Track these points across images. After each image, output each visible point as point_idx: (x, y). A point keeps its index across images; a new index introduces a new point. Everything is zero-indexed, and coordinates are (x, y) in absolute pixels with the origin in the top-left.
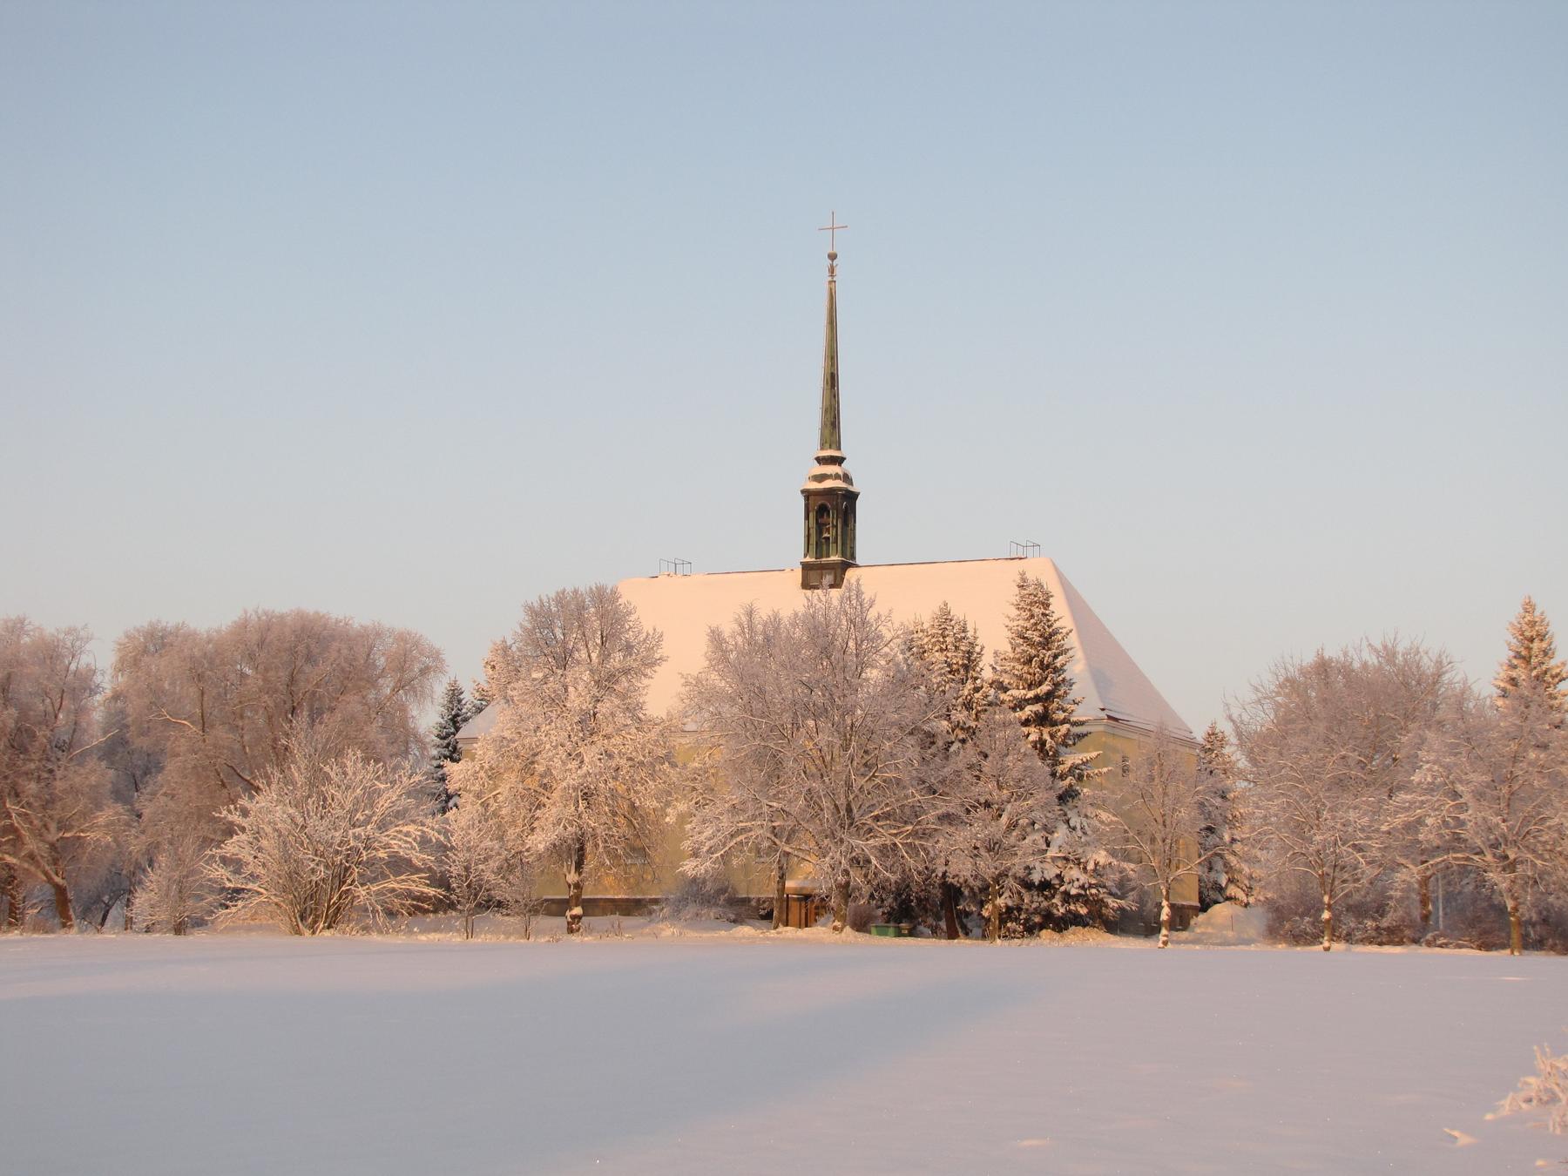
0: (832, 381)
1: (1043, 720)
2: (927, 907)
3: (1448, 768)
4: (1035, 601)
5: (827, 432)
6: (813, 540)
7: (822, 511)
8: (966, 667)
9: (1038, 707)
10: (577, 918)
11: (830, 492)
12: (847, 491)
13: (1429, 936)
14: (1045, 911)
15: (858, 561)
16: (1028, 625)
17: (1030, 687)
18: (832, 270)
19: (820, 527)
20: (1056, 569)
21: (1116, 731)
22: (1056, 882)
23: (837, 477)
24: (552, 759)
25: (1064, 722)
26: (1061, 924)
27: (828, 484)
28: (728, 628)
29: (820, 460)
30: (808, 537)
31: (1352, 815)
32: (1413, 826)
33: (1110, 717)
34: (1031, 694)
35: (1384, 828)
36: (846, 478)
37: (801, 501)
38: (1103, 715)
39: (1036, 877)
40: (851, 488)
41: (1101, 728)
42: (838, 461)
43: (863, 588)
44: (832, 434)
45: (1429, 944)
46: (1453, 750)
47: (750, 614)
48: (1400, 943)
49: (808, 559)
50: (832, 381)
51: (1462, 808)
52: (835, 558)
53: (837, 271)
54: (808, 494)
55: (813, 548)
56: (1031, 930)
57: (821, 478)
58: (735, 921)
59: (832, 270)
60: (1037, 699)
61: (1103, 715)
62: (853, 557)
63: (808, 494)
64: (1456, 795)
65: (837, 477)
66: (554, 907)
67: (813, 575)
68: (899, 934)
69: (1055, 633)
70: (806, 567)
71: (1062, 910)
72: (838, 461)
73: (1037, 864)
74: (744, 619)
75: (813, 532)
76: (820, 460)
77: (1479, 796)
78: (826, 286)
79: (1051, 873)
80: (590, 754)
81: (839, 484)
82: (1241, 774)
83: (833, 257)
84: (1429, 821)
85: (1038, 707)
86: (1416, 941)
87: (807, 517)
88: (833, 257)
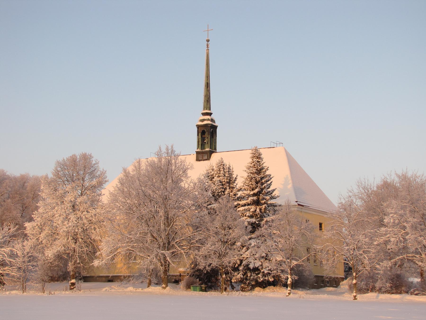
0: (208, 85)
1: (257, 203)
2: (207, 279)
3: (401, 216)
5: (205, 104)
6: (200, 143)
7: (203, 133)
8: (229, 183)
9: (255, 198)
10: (73, 284)
11: (206, 125)
12: (212, 125)
13: (412, 290)
14: (255, 280)
15: (218, 151)
16: (252, 166)
18: (208, 46)
19: (203, 139)
20: (285, 149)
21: (303, 210)
22: (260, 268)
23: (208, 120)
24: (58, 221)
25: (265, 203)
26: (264, 285)
27: (205, 122)
28: (130, 169)
29: (204, 114)
30: (198, 142)
31: (361, 237)
32: (386, 242)
33: (299, 205)
34: (252, 193)
35: (375, 243)
36: (212, 120)
37: (196, 129)
38: (296, 204)
39: (251, 266)
40: (214, 124)
41: (296, 209)
42: (210, 114)
43: (174, 149)
44: (207, 105)
45: (412, 294)
46: (403, 208)
47: (139, 162)
48: (400, 293)
49: (198, 150)
50: (208, 85)
51: (407, 234)
52: (207, 149)
53: (209, 46)
54: (198, 126)
55: (200, 146)
56: (253, 288)
57: (202, 120)
58: (157, 284)
59: (208, 46)
60: (254, 195)
61: (296, 204)
62: (215, 149)
63: (198, 126)
64: (404, 228)
65: (208, 120)
66: (104, 279)
67: (200, 156)
68: (202, 290)
69: (263, 169)
70: (198, 153)
71: (262, 279)
72: (210, 114)
73: (252, 261)
74: (137, 164)
75: (200, 140)
76: (204, 114)
77: (414, 228)
79: (258, 264)
80: (72, 217)
81: (209, 122)
83: (208, 41)
84: (392, 239)
85: (255, 198)
86: (407, 292)
87: (198, 135)
88: (208, 41)
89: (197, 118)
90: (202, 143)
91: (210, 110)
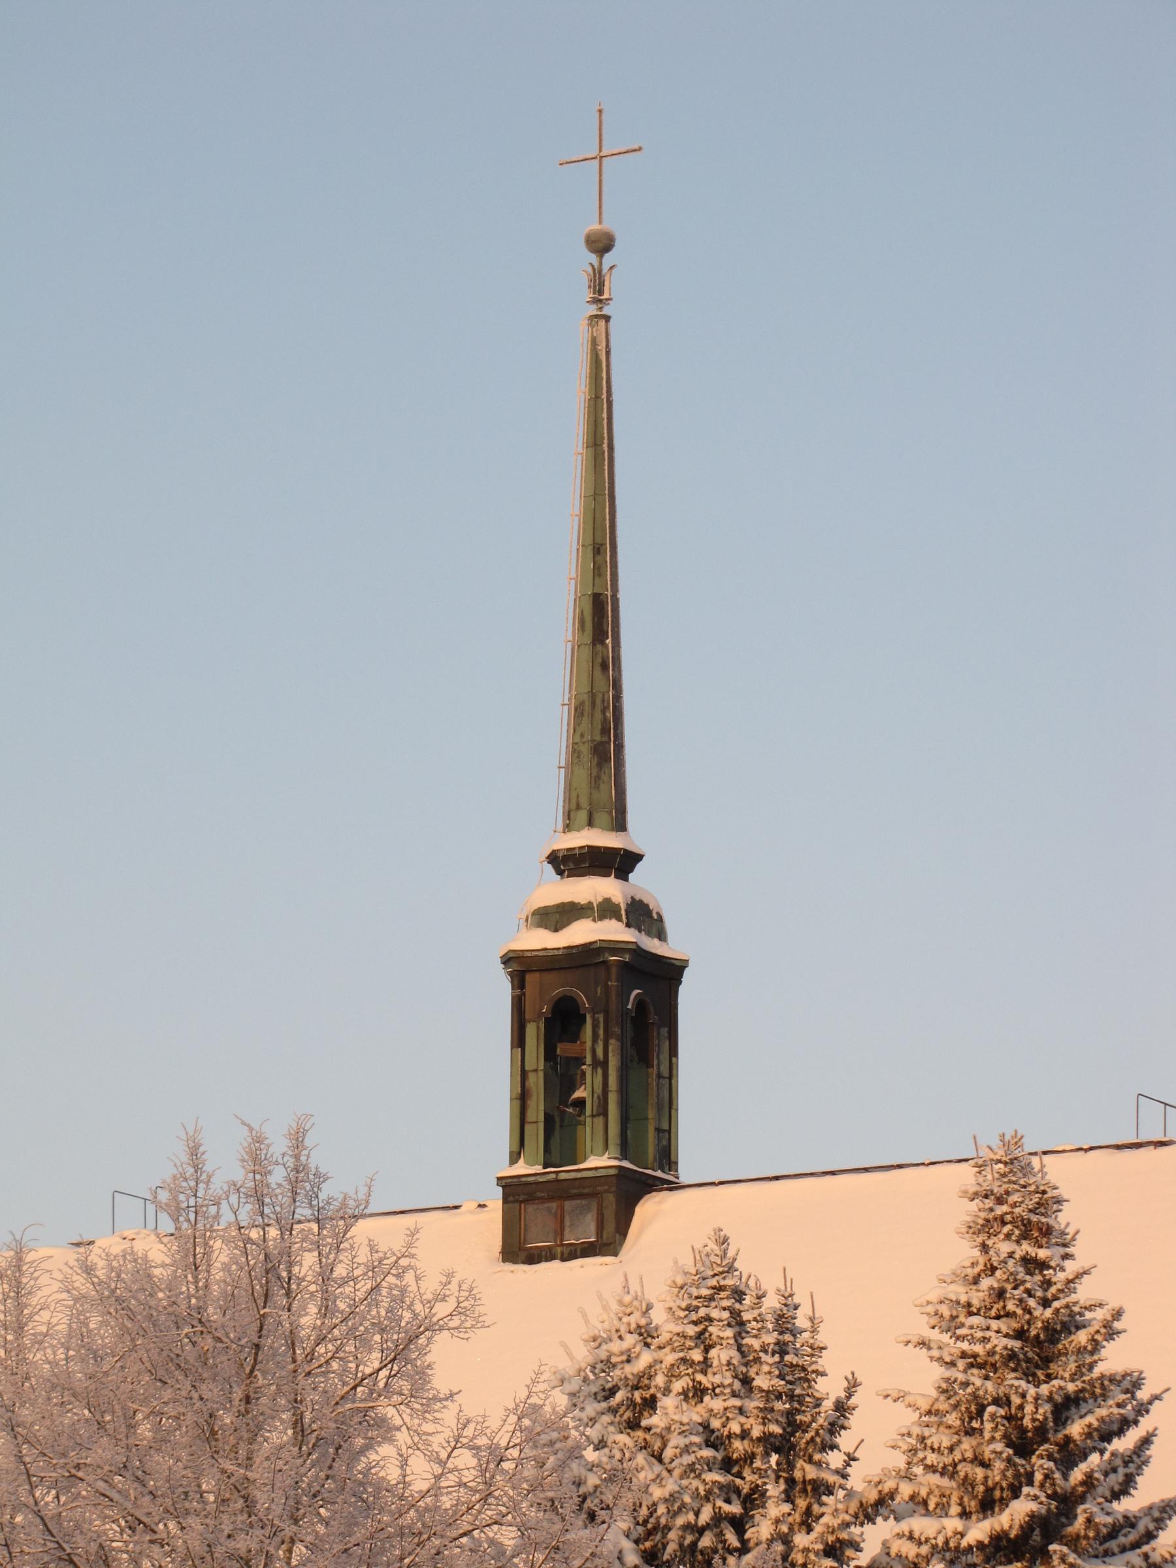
0: (599, 619)
4: (1022, 1218)
5: (582, 774)
6: (537, 1110)
7: (563, 1021)
11: (586, 957)
12: (638, 952)
15: (685, 1173)
16: (977, 1298)
17: (988, 1505)
18: (598, 284)
19: (562, 1075)
23: (607, 910)
27: (581, 933)
29: (567, 863)
30: (522, 1098)
36: (641, 914)
37: (502, 989)
40: (652, 945)
42: (621, 863)
43: (317, 1160)
44: (595, 781)
49: (521, 1168)
50: (599, 619)
53: (614, 286)
54: (522, 968)
55: (536, 1134)
57: (558, 916)
59: (598, 284)
62: (667, 1158)
63: (522, 968)
65: (607, 910)
67: (538, 1217)
70: (515, 1192)
72: (621, 863)
75: (536, 1082)
76: (567, 863)
78: (581, 334)
81: (614, 931)
82: (349, 1467)
83: (601, 244)
87: (519, 1040)
88: (601, 244)
89: (506, 893)
90: (550, 1109)
91: (620, 825)
